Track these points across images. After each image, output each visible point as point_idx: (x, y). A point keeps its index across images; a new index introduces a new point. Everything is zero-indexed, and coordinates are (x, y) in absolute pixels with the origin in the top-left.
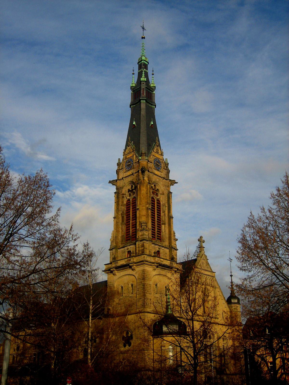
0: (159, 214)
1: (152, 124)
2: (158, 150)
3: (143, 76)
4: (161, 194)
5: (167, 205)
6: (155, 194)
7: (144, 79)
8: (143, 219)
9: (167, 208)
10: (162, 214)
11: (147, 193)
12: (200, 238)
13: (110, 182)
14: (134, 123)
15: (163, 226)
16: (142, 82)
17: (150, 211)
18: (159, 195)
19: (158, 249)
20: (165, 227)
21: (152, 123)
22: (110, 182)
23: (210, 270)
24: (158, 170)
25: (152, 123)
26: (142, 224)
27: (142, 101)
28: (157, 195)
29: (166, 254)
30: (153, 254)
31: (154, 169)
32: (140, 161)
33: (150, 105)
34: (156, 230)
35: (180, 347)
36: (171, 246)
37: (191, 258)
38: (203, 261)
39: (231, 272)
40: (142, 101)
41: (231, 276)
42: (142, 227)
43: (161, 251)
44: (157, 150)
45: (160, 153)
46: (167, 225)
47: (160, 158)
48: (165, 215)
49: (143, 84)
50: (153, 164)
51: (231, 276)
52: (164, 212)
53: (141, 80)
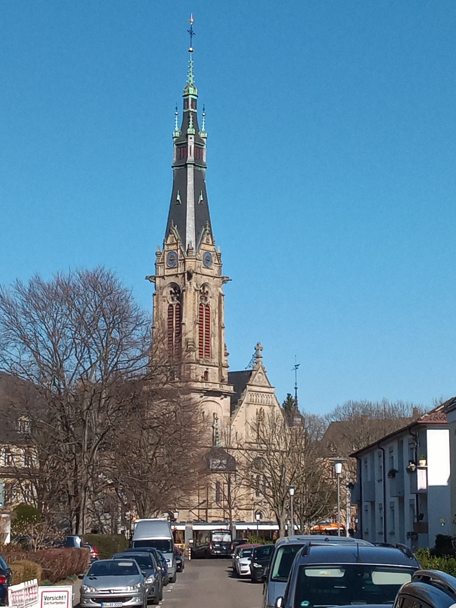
0: (208, 326)
1: (201, 201)
2: (209, 240)
3: (191, 126)
4: (211, 297)
5: (217, 311)
6: (204, 298)
7: (191, 130)
8: (190, 335)
9: (217, 315)
10: (211, 324)
11: (194, 304)
12: (258, 345)
13: (147, 278)
14: (178, 198)
15: (212, 338)
16: (189, 136)
17: (197, 326)
18: (209, 299)
19: (206, 370)
20: (214, 340)
21: (202, 199)
22: (147, 278)
23: (268, 385)
24: (208, 268)
25: (202, 199)
26: (189, 343)
27: (188, 165)
28: (206, 299)
29: (215, 373)
30: (200, 379)
31: (203, 267)
32: (186, 260)
33: (199, 169)
34: (204, 324)
35: (20, 359)
36: (221, 364)
37: (246, 368)
38: (260, 375)
39: (296, 384)
40: (188, 165)
41: (296, 388)
42: (189, 346)
43: (209, 371)
44: (208, 239)
45: (211, 243)
46: (217, 338)
47: (211, 250)
48: (214, 324)
49: (191, 138)
50: (202, 262)
51: (296, 388)
52: (214, 321)
53: (188, 133)
